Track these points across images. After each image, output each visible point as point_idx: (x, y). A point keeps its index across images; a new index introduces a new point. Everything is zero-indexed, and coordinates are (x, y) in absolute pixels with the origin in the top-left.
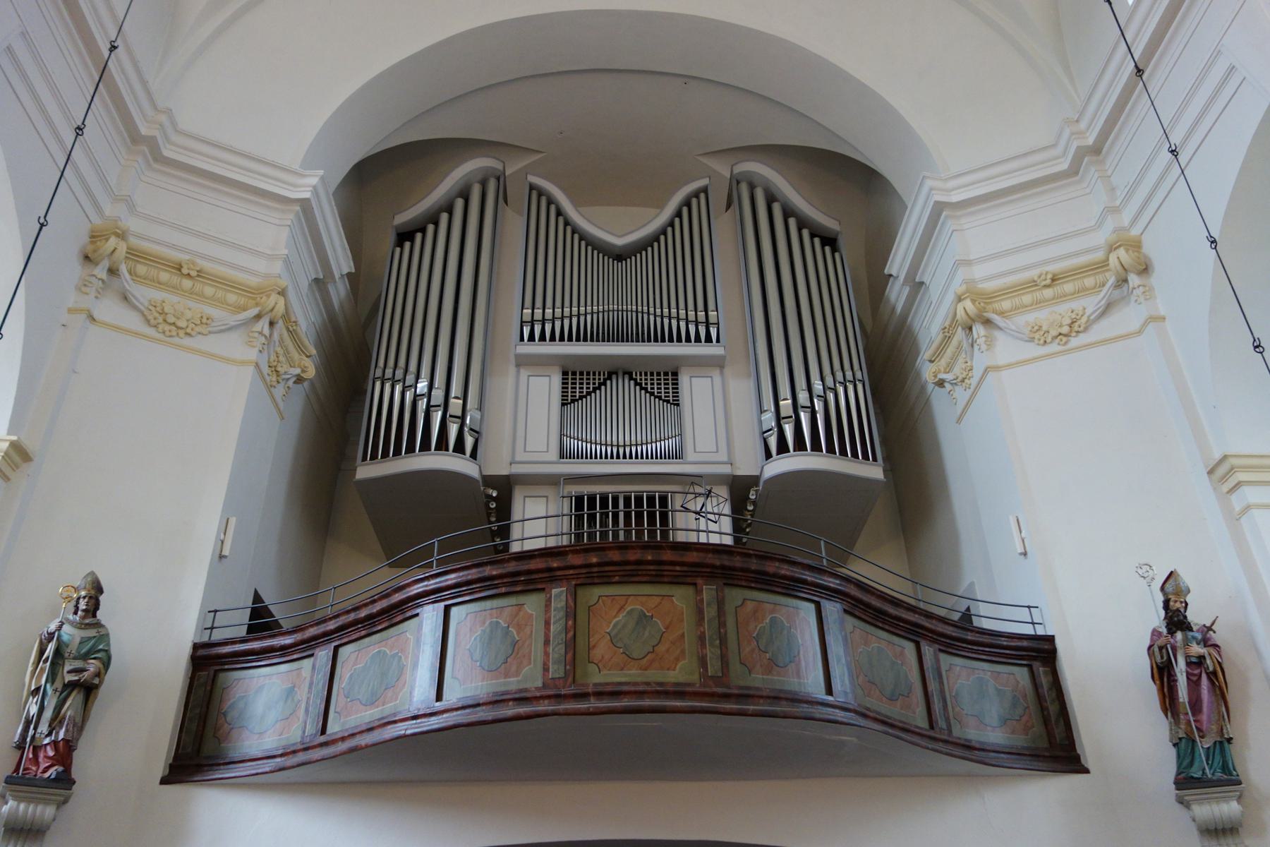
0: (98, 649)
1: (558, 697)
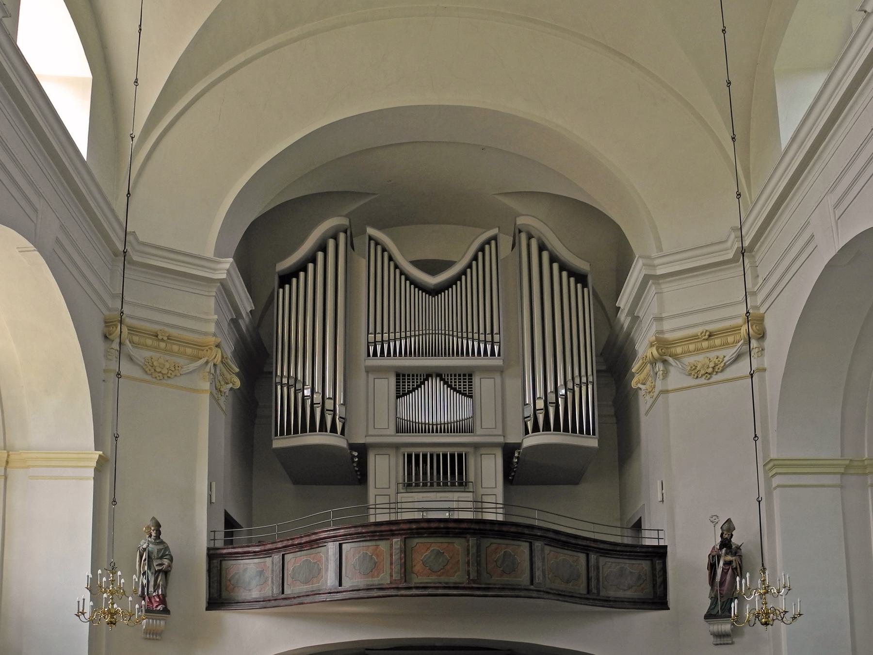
0: (165, 552)
1: (398, 588)
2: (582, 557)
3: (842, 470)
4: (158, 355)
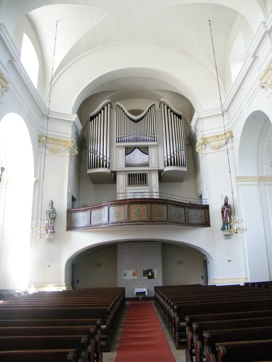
1: (127, 222)
2: (183, 209)
3: (258, 180)
4: (54, 145)
